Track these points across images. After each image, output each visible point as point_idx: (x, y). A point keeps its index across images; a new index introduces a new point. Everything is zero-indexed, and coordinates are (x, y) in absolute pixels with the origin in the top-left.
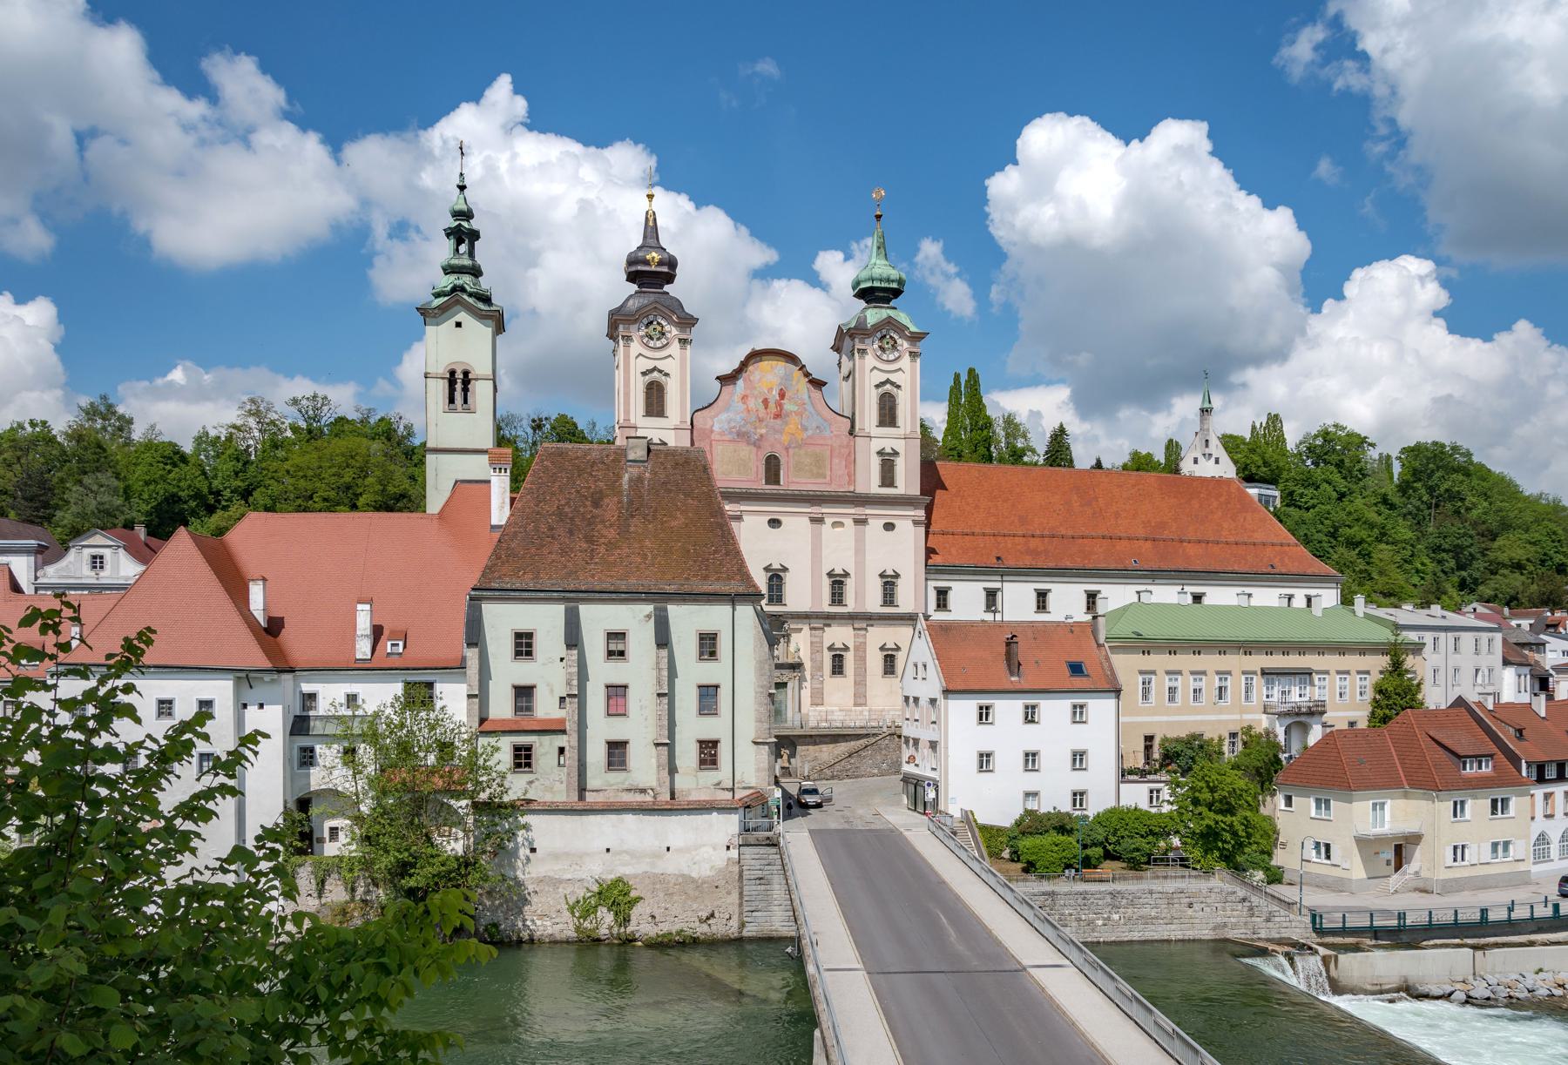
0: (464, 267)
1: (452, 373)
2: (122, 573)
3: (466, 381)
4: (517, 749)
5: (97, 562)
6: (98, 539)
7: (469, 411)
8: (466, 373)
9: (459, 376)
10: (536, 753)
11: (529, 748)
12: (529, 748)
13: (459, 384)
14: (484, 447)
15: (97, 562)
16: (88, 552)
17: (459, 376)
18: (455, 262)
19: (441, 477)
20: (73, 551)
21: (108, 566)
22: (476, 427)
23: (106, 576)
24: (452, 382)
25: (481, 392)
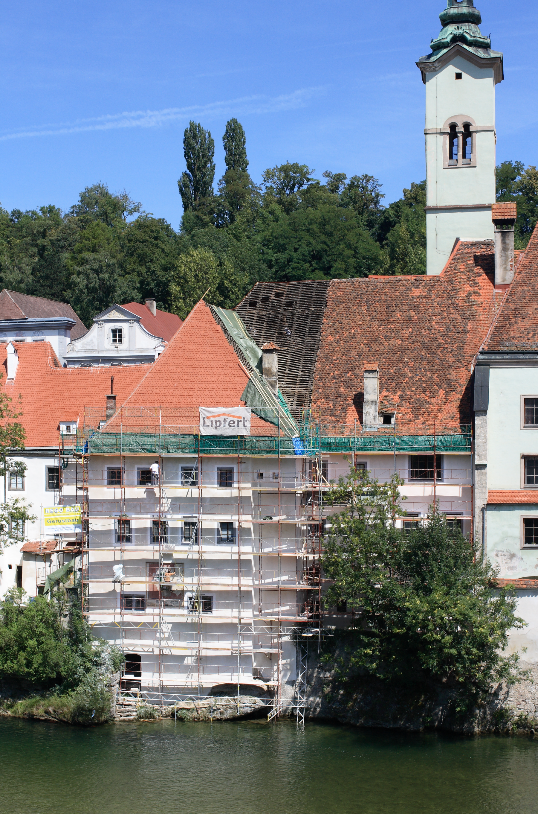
0: (463, 15)
1: (453, 126)
2: (138, 346)
3: (468, 133)
4: (114, 331)
5: (117, 335)
6: (114, 315)
7: (469, 165)
8: (467, 126)
9: (460, 129)
10: (125, 333)
11: (120, 331)
12: (120, 331)
13: (460, 136)
14: (486, 203)
15: (117, 335)
16: (109, 327)
17: (460, 129)
18: (454, 11)
19: (441, 240)
20: (95, 326)
21: (125, 339)
22: (478, 183)
23: (124, 349)
24: (453, 134)
25: (485, 148)
